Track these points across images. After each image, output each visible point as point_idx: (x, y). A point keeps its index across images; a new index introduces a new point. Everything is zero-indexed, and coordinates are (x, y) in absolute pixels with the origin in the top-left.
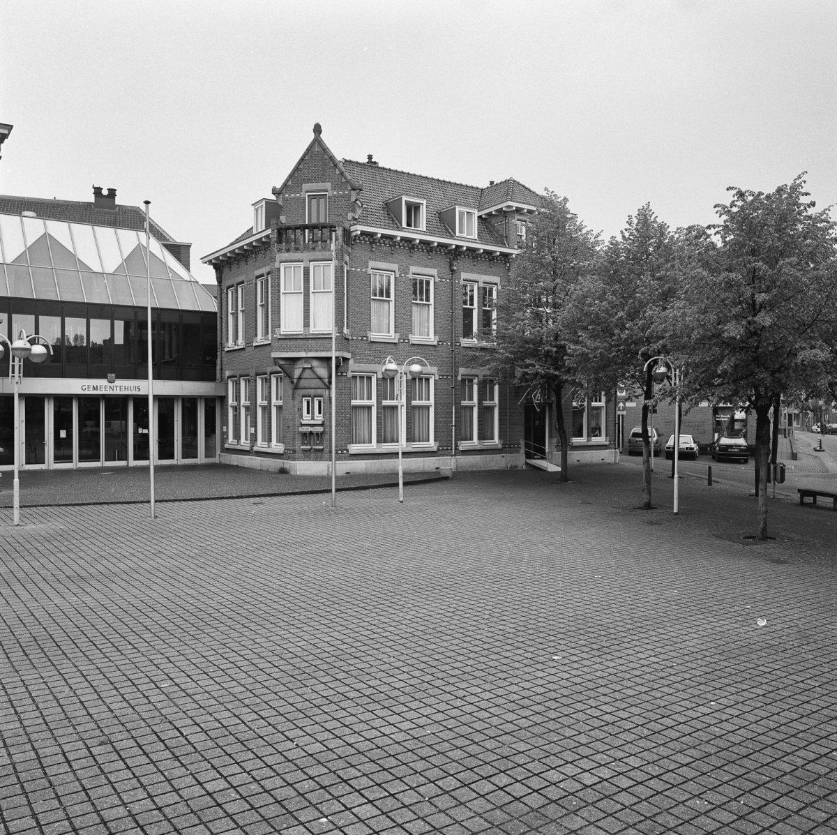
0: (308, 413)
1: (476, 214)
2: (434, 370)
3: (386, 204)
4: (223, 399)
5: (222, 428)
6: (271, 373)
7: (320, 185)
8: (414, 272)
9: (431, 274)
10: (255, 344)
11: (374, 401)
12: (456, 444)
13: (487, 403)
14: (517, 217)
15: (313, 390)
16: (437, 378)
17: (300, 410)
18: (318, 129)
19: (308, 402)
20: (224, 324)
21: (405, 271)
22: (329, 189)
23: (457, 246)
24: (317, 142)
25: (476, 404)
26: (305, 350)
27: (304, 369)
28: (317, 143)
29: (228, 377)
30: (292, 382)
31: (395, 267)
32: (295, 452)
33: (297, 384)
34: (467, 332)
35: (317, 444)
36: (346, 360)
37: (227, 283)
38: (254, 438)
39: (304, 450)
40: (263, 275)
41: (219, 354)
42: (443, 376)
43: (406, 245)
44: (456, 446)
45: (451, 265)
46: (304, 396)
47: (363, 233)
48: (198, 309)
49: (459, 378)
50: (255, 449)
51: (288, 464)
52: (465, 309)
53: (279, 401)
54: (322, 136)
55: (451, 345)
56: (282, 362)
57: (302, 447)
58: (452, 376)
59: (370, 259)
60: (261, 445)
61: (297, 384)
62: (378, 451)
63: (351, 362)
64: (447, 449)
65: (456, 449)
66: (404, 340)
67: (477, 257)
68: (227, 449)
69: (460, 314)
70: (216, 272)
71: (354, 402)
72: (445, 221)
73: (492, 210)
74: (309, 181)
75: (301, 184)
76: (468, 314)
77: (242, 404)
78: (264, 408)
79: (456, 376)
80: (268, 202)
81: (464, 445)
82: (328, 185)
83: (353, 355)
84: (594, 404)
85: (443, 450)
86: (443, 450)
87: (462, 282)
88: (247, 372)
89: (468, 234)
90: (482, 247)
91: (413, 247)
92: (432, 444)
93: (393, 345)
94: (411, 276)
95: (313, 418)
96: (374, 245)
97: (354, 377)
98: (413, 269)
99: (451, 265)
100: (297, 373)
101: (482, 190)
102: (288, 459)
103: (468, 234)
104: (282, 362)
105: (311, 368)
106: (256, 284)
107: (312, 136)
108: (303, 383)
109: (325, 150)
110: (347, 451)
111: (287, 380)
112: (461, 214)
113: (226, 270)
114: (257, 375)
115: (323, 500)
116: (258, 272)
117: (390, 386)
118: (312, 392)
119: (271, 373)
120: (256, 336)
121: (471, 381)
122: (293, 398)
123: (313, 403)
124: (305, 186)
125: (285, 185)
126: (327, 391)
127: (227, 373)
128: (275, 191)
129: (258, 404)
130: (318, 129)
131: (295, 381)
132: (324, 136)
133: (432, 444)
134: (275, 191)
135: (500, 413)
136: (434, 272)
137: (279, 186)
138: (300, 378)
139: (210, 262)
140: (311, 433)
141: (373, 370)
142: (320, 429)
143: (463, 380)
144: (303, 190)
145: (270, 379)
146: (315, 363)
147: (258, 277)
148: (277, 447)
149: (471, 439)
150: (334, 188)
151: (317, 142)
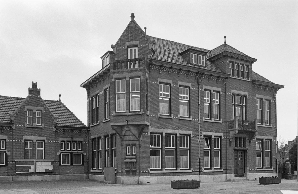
14: (229, 60)
18: (133, 16)
22: (139, 44)
24: (133, 22)
27: (127, 130)
35: (133, 168)
39: (126, 171)
54: (135, 19)
56: (115, 128)
57: (126, 169)
59: (159, 77)
62: (185, 135)
63: (150, 127)
68: (92, 172)
70: (87, 91)
75: (125, 42)
79: (201, 136)
80: (109, 52)
83: (151, 124)
85: (195, 171)
86: (195, 171)
101: (210, 51)
105: (130, 130)
107: (130, 19)
113: (91, 90)
115: (230, 182)
118: (131, 143)
125: (117, 43)
126: (138, 142)
128: (112, 47)
130: (133, 16)
131: (122, 137)
132: (135, 19)
134: (112, 47)
137: (114, 44)
138: (124, 135)
139: (84, 87)
140: (130, 162)
142: (135, 160)
146: (131, 128)
151: (133, 22)
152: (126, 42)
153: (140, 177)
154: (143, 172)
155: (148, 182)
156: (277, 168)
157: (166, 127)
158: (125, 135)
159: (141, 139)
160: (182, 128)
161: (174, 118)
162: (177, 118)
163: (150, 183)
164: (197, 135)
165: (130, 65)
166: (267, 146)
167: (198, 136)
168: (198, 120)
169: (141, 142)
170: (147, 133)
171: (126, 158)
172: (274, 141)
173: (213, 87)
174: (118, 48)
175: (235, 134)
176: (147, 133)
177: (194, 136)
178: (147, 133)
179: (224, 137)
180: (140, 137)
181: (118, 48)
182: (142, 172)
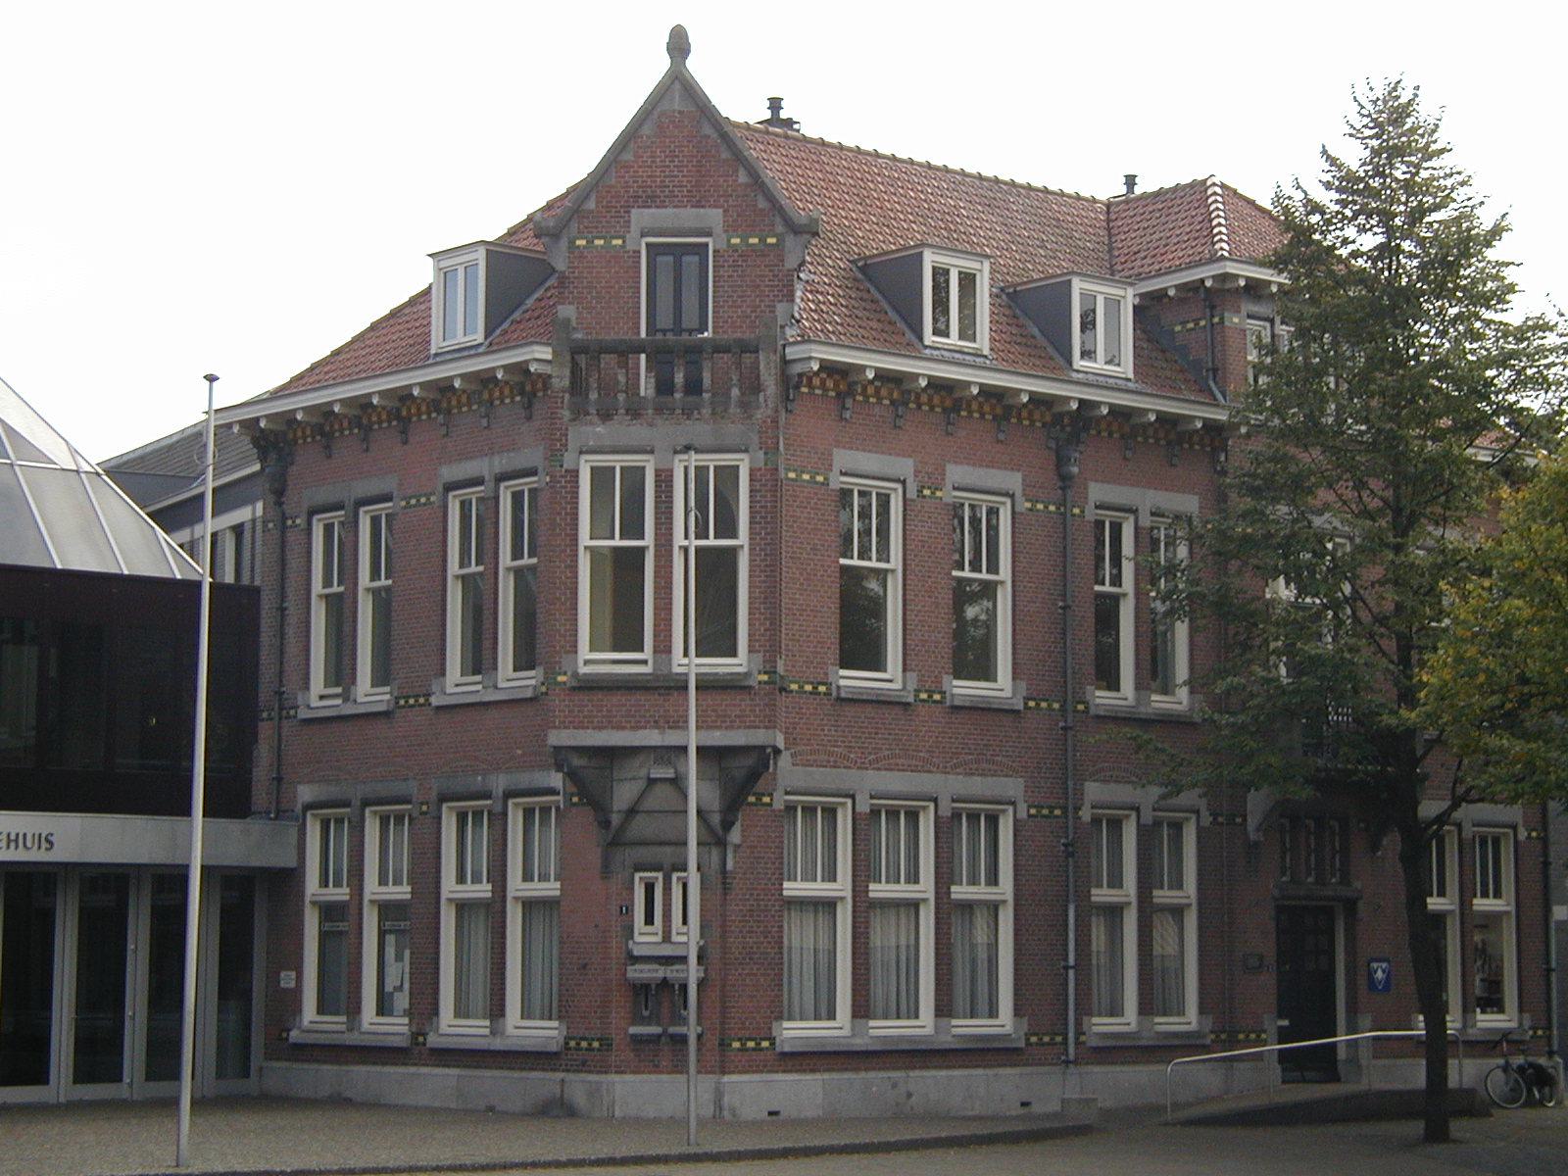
0: (649, 919)
1: (1129, 297)
2: (1012, 787)
3: (861, 269)
4: (284, 881)
5: (273, 978)
6: (509, 794)
7: (688, 216)
8: (849, 466)
9: (1004, 487)
10: (435, 701)
11: (926, 887)
12: (1078, 1023)
13: (1163, 896)
14: (1248, 307)
15: (668, 850)
16: (1022, 814)
17: (627, 911)
18: (679, 45)
19: (650, 889)
20: (290, 631)
21: (932, 479)
22: (718, 229)
23: (1082, 402)
25: (1133, 899)
26: (656, 725)
27: (652, 782)
28: (677, 86)
29: (308, 807)
30: (606, 824)
31: (905, 467)
32: (606, 1044)
33: (623, 827)
34: (862, 649)
36: (762, 758)
37: (301, 497)
38: (425, 1007)
39: (637, 1040)
40: (478, 481)
41: (265, 730)
42: (1039, 807)
43: (830, 384)
44: (1079, 1032)
45: (1061, 461)
46: (639, 868)
47: (828, 368)
48: (114, 570)
49: (1086, 815)
50: (433, 1040)
51: (578, 1086)
52: (845, 569)
53: (391, 888)
55: (1063, 709)
56: (577, 761)
57: (633, 1030)
58: (1065, 809)
59: (838, 444)
60: (452, 1026)
61: (623, 827)
63: (784, 761)
64: (1052, 1043)
65: (1078, 1043)
66: (930, 693)
67: (1006, 417)
69: (1085, 614)
71: (793, 888)
72: (1036, 318)
73: (1170, 282)
74: (651, 200)
76: (1106, 613)
77: (367, 896)
78: (330, 912)
79: (1077, 809)
81: (1101, 1025)
82: (714, 217)
84: (1481, 904)
86: (1040, 1043)
87: (1091, 514)
88: (398, 788)
89: (1106, 361)
90: (1153, 405)
91: (957, 406)
92: (1004, 1022)
93: (898, 710)
94: (948, 495)
95: (667, 937)
96: (849, 403)
97: (791, 809)
98: (956, 473)
99: (1061, 461)
100: (624, 795)
102: (583, 1067)
103: (1106, 361)
104: (577, 761)
106: (445, 507)
107: (663, 64)
108: (641, 827)
109: (702, 108)
110: (772, 1041)
111: (585, 816)
112: (941, 275)
114: (443, 798)
116: (451, 472)
117: (805, 834)
119: (509, 794)
120: (442, 672)
121: (1116, 825)
122: (606, 871)
123: (667, 889)
124: (640, 217)
127: (306, 793)
129: (445, 894)
130: (679, 45)
131: (616, 819)
132: (694, 65)
133: (1004, 1022)
135: (1201, 928)
136: (1013, 481)
138: (632, 812)
141: (845, 786)
143: (1096, 821)
144: (634, 229)
145: (505, 814)
147: (450, 487)
148: (524, 1029)
149: (1181, 1012)
150: (731, 228)
152: (634, 211)
153: (726, 1078)
154: (743, 1049)
155: (771, 1113)
156: (1549, 1027)
157: (877, 760)
158: (636, 808)
159: (735, 836)
160: (1102, 770)
161: (924, 696)
162: (937, 697)
163: (781, 1117)
164: (1051, 808)
165: (881, 510)
166: (1484, 868)
167: (1057, 812)
168: (1056, 706)
169: (735, 851)
170: (766, 799)
171: (636, 953)
172: (1529, 837)
173: (1151, 493)
174: (578, 242)
175: (1192, 611)
176: (766, 799)
177: (1033, 811)
178: (771, 795)
179: (1215, 816)
180: (727, 825)
181: (578, 242)
182: (736, 1045)
